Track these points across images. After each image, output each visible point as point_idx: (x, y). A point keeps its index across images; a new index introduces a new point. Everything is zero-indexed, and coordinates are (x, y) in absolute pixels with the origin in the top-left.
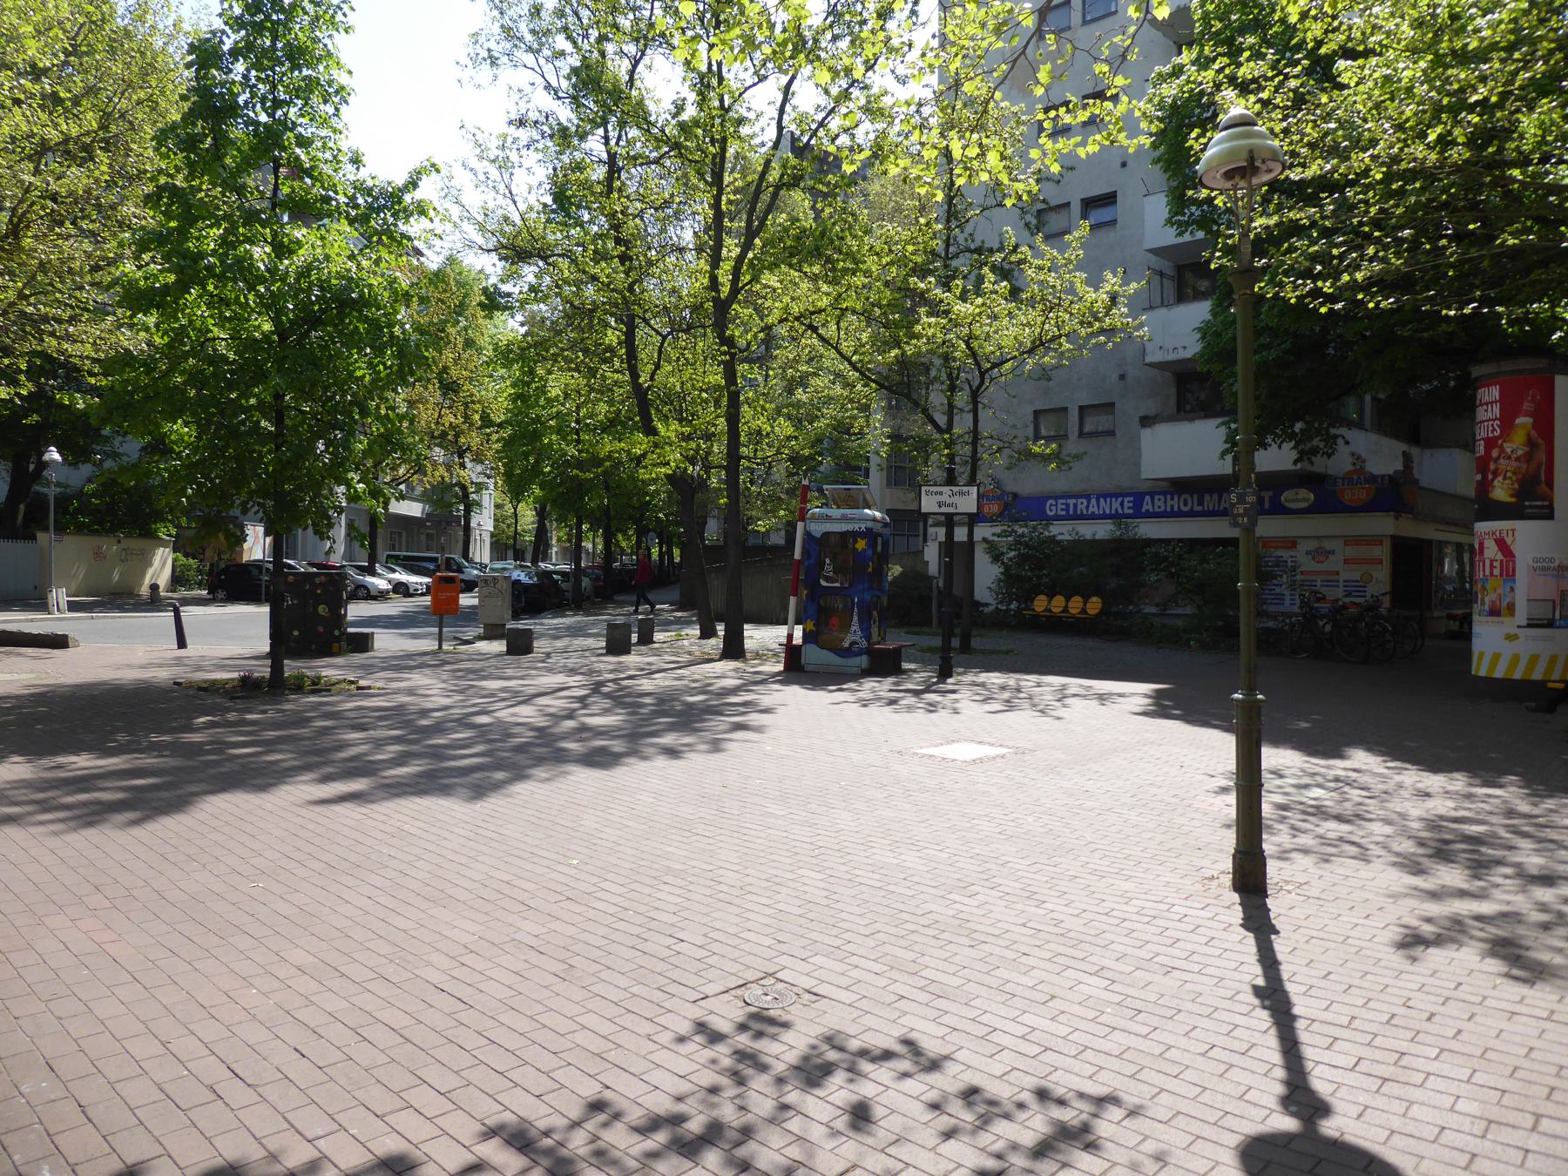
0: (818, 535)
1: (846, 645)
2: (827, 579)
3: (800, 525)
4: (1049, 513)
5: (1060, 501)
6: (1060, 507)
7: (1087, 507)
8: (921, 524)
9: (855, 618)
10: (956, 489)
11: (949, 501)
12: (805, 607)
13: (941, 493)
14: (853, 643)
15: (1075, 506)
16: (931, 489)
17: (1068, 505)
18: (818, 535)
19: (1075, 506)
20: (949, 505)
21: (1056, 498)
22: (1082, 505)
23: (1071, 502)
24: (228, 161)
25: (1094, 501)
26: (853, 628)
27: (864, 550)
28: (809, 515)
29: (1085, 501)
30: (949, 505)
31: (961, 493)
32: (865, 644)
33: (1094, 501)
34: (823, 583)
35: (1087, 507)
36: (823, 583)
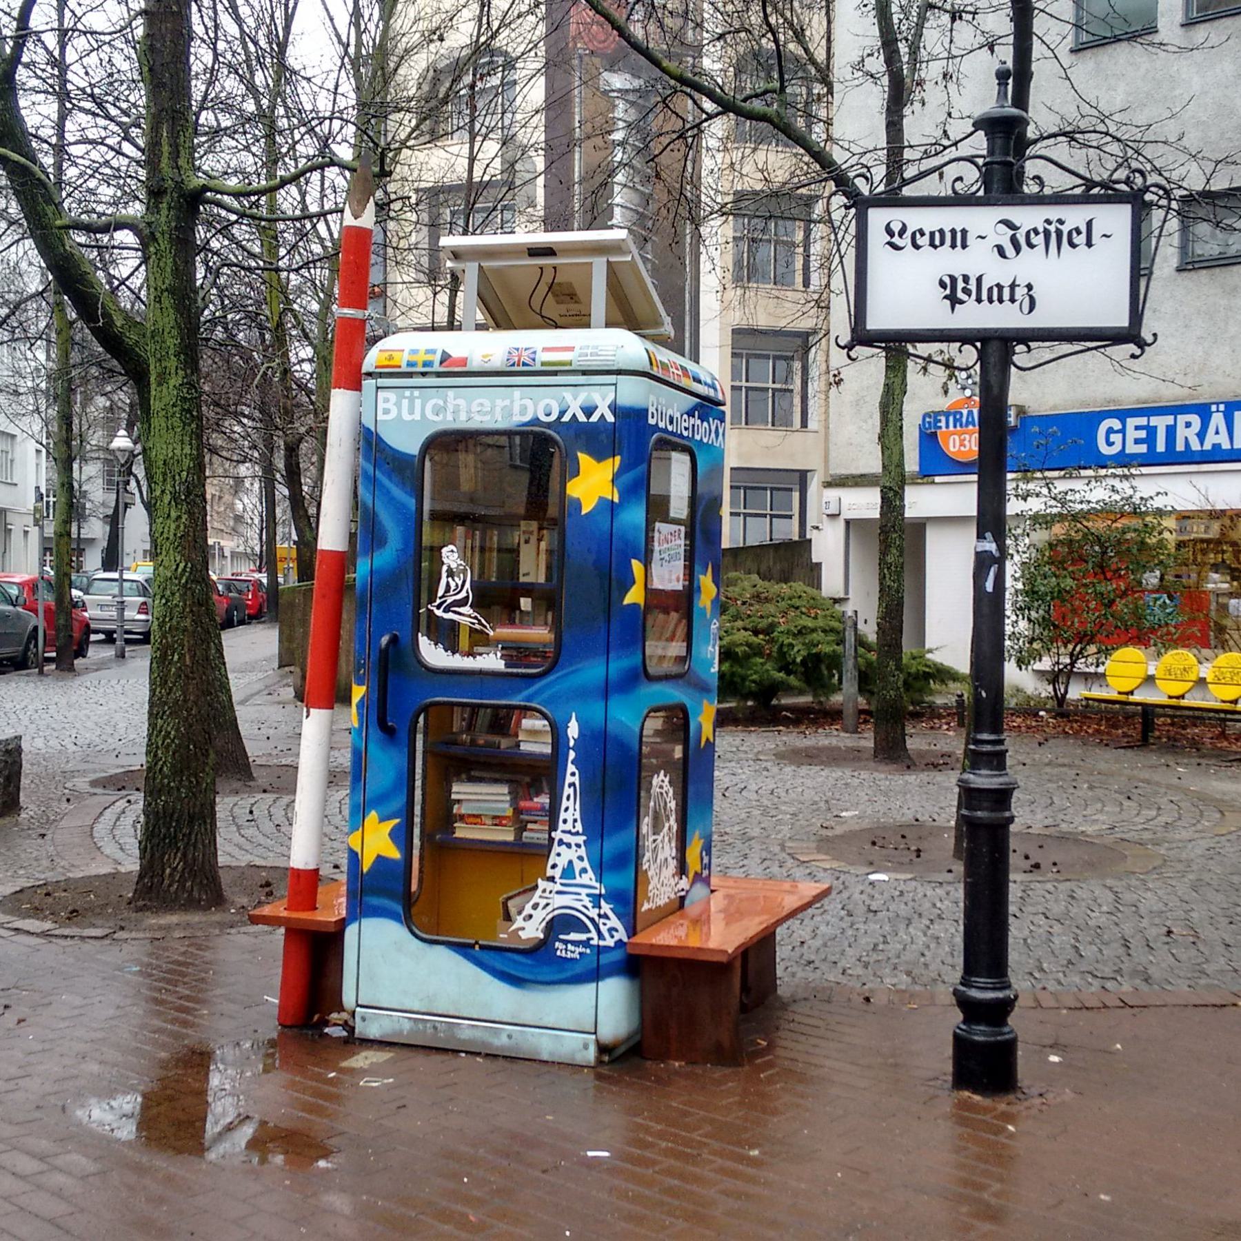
0: (410, 445)
1: (530, 929)
2: (447, 635)
3: (341, 402)
4: (1105, 450)
5: (1132, 422)
6: (1132, 434)
7: (1201, 435)
8: (796, 496)
9: (571, 812)
10: (1028, 218)
11: (997, 272)
12: (359, 759)
13: (959, 239)
14: (561, 924)
15: (1171, 431)
16: (917, 219)
17: (1152, 431)
18: (410, 445)
19: (1171, 431)
20: (997, 294)
21: (1122, 415)
22: (1187, 432)
23: (1161, 423)
24: (307, 352)
25: (1217, 419)
26: (561, 857)
27: (609, 508)
28: (373, 359)
29: (1195, 420)
30: (997, 294)
31: (1057, 238)
32: (612, 931)
33: (1217, 419)
34: (433, 654)
35: (1201, 435)
36: (433, 654)
